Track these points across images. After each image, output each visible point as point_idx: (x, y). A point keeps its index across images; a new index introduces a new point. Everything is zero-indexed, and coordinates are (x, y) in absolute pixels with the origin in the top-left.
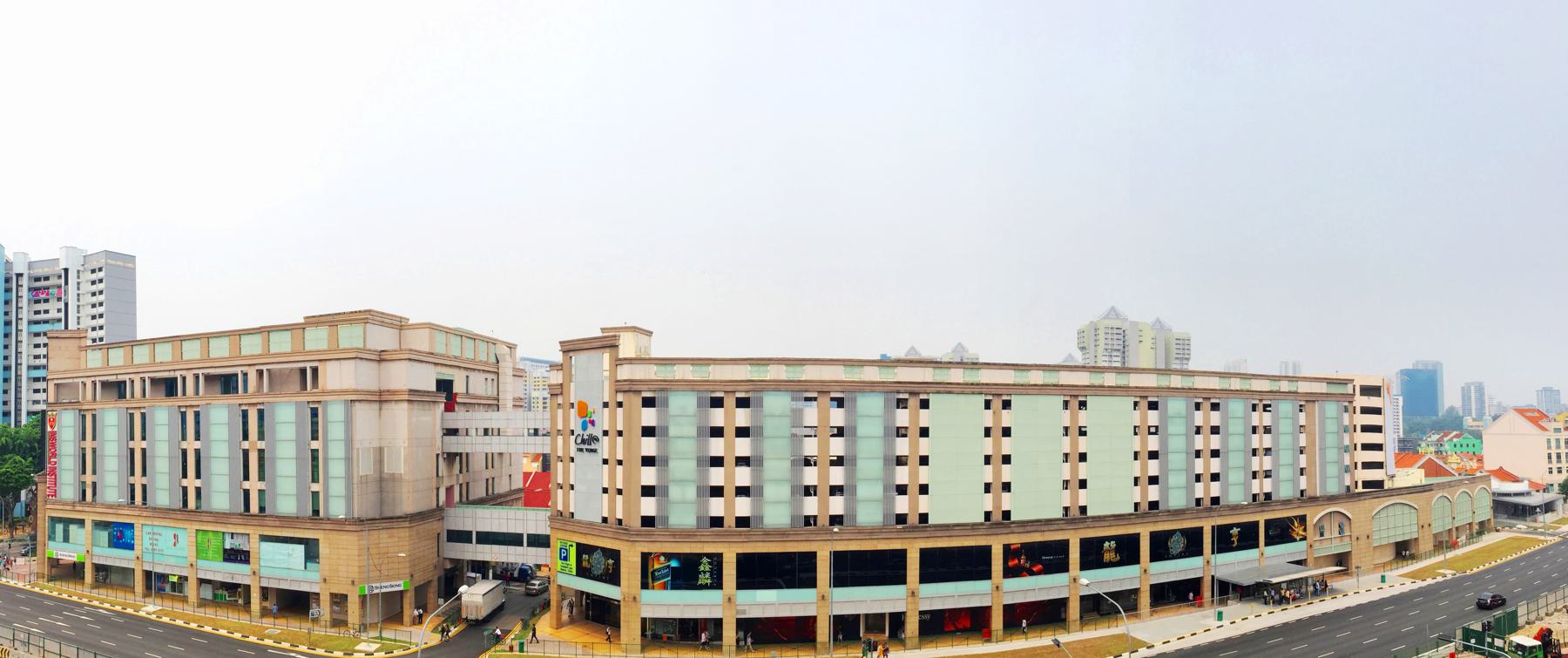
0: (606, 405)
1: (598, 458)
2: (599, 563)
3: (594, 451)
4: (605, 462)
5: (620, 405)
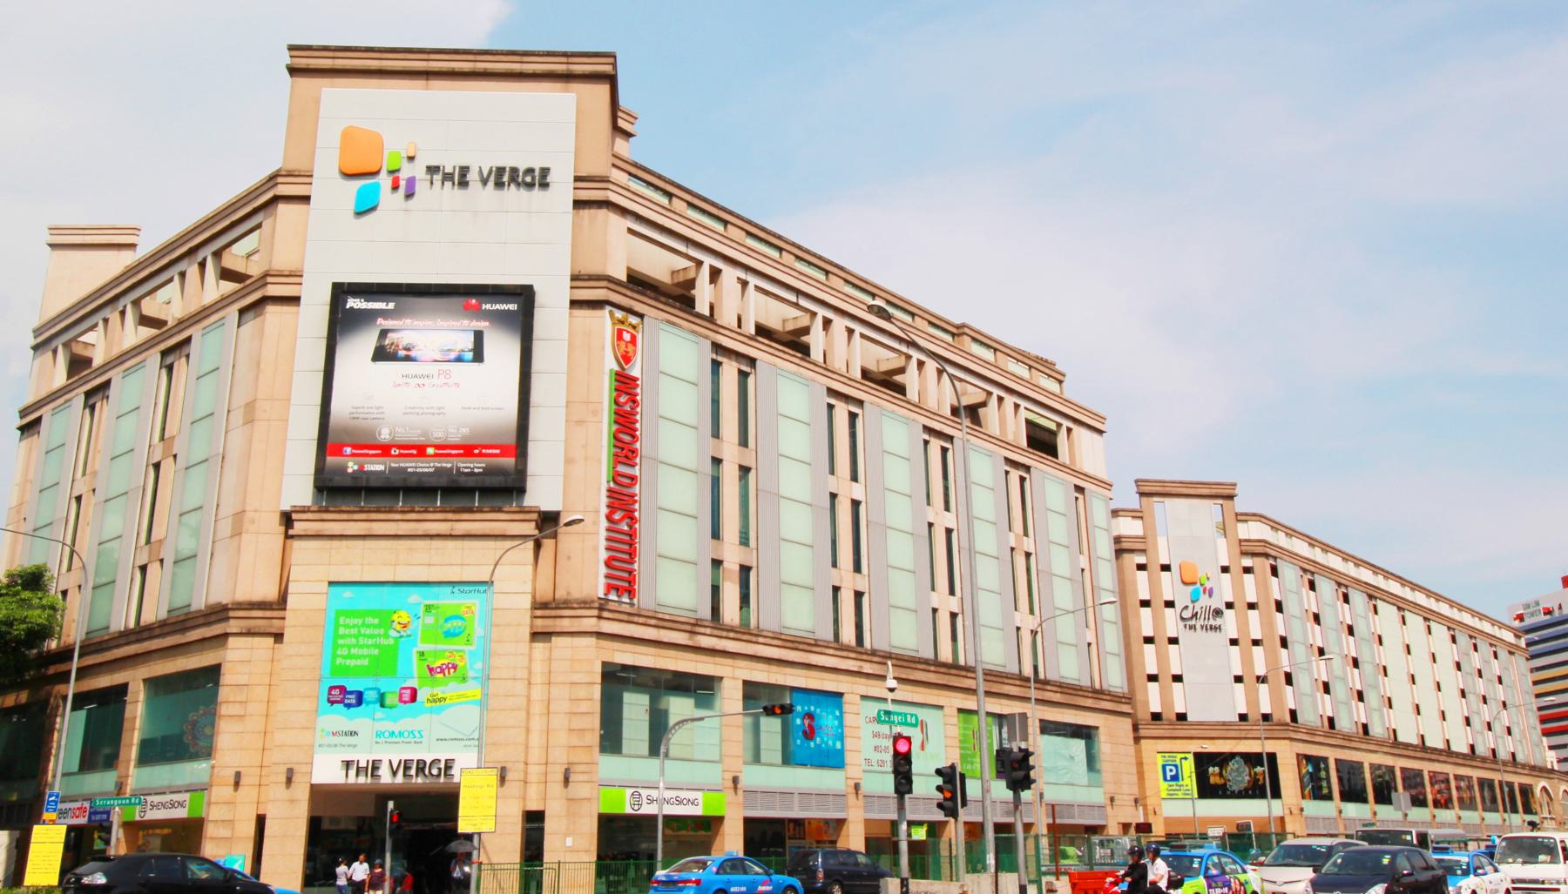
0: (1225, 569)
1: (1221, 639)
2: (1238, 775)
3: (1217, 628)
4: (1234, 642)
5: (1247, 570)
